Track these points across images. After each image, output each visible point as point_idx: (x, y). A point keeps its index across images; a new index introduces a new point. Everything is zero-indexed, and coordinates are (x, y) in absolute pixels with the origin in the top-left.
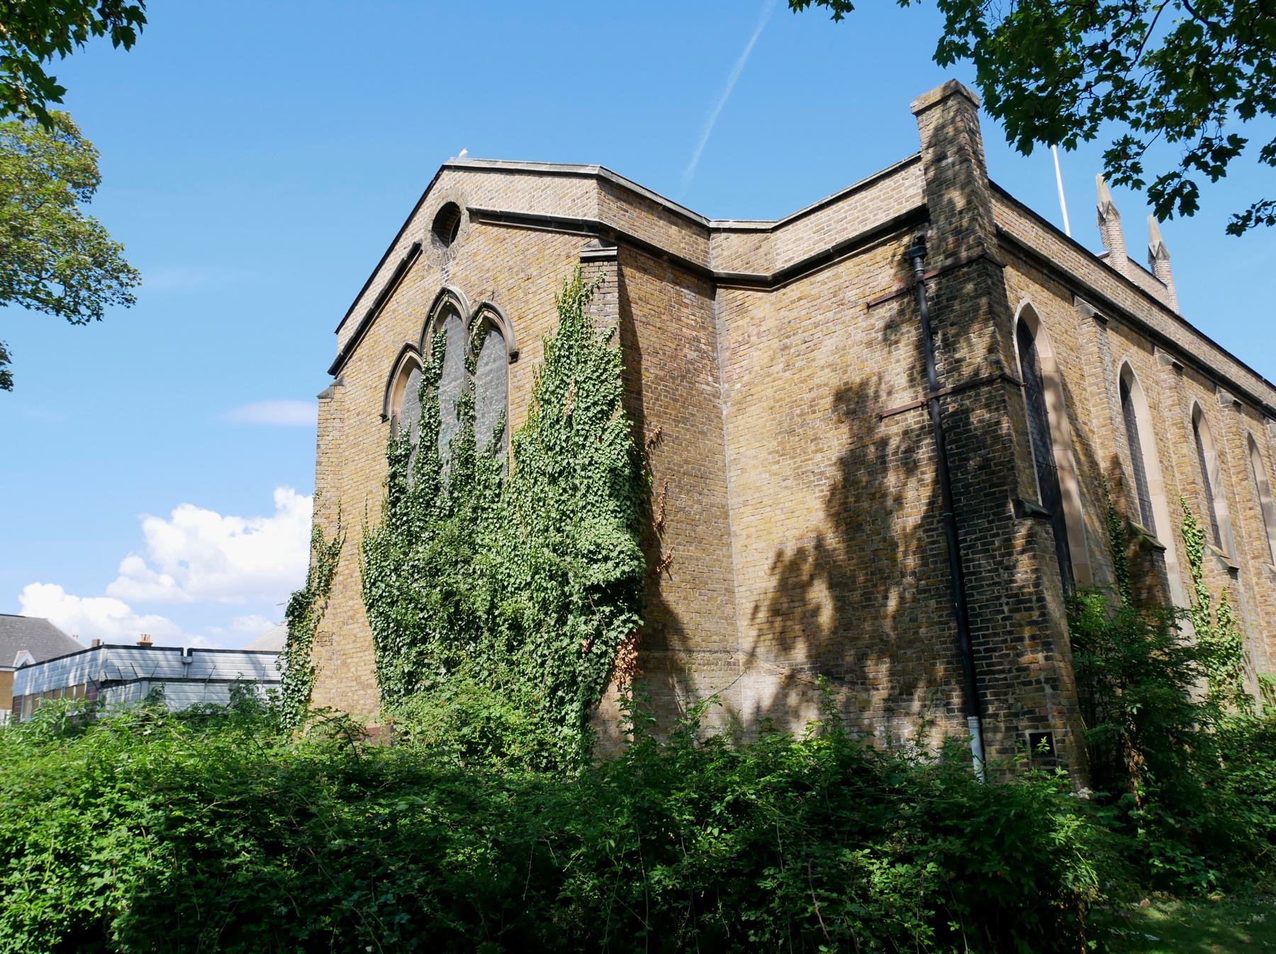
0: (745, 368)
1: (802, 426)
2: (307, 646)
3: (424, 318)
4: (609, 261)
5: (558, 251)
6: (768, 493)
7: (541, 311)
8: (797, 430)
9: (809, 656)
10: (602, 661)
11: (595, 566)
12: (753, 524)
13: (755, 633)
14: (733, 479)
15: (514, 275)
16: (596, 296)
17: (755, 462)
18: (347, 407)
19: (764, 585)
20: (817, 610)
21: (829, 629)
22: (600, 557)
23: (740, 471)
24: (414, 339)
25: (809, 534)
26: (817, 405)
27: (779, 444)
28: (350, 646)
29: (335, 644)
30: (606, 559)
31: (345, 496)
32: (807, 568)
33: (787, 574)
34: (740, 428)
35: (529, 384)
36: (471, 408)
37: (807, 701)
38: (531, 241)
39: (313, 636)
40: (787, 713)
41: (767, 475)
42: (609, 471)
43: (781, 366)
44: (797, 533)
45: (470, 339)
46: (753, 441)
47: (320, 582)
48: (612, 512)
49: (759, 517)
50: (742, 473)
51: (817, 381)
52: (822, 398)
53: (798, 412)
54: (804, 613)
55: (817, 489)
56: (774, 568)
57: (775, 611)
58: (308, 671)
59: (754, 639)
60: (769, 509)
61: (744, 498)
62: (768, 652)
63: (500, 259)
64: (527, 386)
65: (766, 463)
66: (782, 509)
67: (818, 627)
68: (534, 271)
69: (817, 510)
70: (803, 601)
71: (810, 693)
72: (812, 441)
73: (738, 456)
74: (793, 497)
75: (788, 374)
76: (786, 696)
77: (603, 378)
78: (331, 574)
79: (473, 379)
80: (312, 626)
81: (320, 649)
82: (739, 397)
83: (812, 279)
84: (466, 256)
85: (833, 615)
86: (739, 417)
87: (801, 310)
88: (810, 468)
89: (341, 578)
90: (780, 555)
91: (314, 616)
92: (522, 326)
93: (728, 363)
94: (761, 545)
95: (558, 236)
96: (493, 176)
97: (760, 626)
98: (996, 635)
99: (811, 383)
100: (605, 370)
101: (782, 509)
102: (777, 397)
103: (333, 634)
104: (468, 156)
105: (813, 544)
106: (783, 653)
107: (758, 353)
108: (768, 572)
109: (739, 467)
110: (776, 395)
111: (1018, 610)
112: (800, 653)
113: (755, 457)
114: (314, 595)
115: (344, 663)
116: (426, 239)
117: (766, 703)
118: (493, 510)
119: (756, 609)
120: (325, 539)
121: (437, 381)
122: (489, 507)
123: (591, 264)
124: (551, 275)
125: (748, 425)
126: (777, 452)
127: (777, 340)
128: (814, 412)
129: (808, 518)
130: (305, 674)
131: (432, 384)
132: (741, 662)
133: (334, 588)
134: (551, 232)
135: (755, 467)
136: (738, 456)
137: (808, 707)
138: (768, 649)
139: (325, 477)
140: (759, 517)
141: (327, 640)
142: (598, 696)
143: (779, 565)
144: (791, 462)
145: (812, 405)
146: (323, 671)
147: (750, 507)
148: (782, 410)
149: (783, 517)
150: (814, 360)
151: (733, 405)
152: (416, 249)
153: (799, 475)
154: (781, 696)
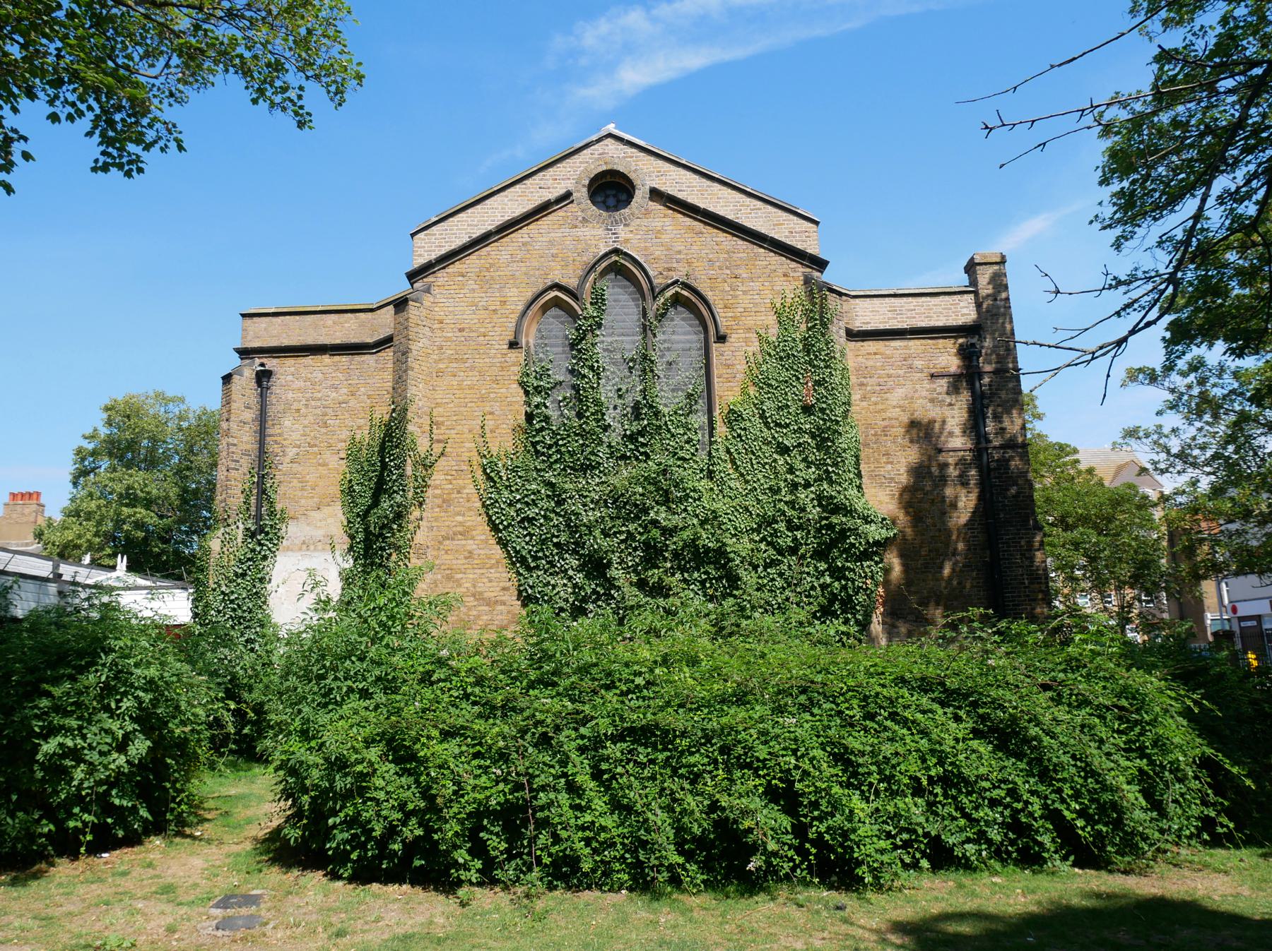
5: (773, 267)
7: (754, 309)
24: (572, 283)
31: (441, 409)
43: (859, 396)
52: (893, 427)
68: (743, 273)
75: (864, 404)
83: (887, 343)
87: (877, 362)
89: (438, 492)
92: (730, 314)
95: (772, 254)
98: (1020, 596)
99: (884, 415)
111: (1033, 583)
116: (578, 191)
124: (766, 284)
145: (885, 429)
152: (567, 196)
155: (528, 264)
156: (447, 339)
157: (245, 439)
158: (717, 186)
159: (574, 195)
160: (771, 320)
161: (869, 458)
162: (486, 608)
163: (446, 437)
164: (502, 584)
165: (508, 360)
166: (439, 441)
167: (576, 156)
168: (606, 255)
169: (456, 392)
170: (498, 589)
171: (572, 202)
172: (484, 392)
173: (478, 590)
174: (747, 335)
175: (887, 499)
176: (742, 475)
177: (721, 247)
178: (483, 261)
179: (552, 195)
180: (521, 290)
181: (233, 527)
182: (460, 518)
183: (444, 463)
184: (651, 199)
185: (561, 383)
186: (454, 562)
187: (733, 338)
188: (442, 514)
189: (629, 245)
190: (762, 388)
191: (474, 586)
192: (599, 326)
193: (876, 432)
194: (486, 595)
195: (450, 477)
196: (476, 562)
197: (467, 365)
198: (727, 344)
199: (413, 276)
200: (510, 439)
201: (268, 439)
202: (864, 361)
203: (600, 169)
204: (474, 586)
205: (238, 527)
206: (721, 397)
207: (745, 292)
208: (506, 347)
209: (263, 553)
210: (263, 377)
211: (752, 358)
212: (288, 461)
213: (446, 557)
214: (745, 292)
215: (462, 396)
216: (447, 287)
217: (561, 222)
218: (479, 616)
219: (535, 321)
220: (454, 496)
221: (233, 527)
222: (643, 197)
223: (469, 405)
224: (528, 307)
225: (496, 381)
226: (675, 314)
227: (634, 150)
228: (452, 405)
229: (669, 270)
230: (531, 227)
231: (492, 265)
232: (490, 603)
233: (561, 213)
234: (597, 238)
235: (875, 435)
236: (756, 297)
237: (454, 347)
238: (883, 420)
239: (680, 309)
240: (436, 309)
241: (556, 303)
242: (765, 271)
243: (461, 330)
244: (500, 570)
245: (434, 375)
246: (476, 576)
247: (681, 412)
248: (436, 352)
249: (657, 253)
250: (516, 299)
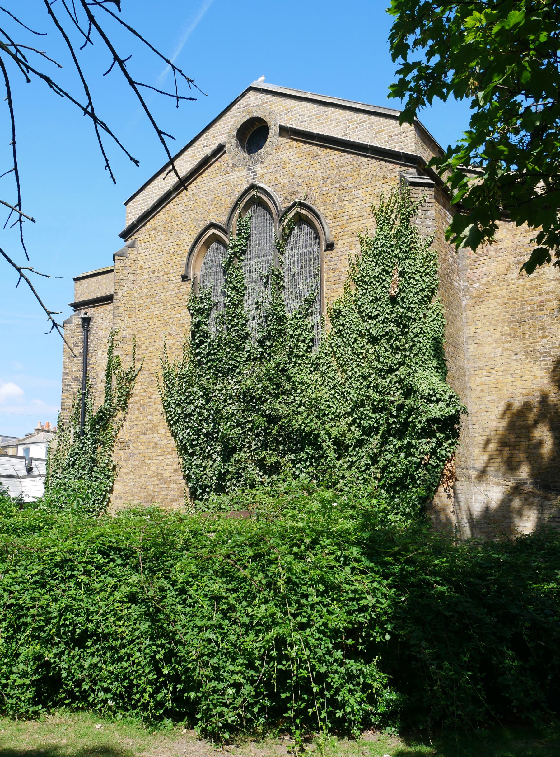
0: (483, 273)
1: (531, 319)
2: (110, 449)
3: (230, 206)
4: (429, 187)
5: (375, 173)
6: (500, 362)
7: (357, 215)
8: (527, 321)
9: (531, 475)
10: (436, 470)
11: (432, 405)
12: (486, 383)
13: (486, 457)
14: (469, 350)
15: (328, 184)
16: (420, 212)
17: (490, 340)
18: (139, 265)
19: (494, 425)
20: (540, 444)
21: (548, 457)
22: (435, 398)
23: (476, 345)
24: (222, 220)
25: (534, 393)
26: (545, 305)
27: (511, 329)
28: (149, 451)
29: (131, 448)
30: (438, 401)
31: (140, 335)
32: (532, 416)
33: (515, 419)
34: (477, 315)
35: (345, 269)
36: (282, 280)
37: (528, 504)
38: (346, 161)
39: (114, 441)
40: (511, 512)
41: (500, 350)
42: (433, 339)
44: (524, 391)
45: (281, 228)
46: (488, 325)
47: (120, 401)
48: (435, 368)
49: (492, 378)
50: (478, 346)
51: (545, 289)
53: (529, 308)
54: (528, 446)
55: (543, 363)
56: (504, 414)
57: (503, 443)
58: (110, 468)
59: (486, 461)
60: (501, 373)
61: (479, 364)
62: (498, 470)
63: (312, 169)
64: (343, 269)
65: (499, 341)
66: (512, 374)
67: (540, 456)
68: (350, 184)
69: (541, 377)
70: (529, 439)
71: (531, 499)
72: (539, 329)
73: (475, 334)
74: (522, 367)
76: (511, 500)
77: (427, 272)
78: (128, 394)
79: (281, 257)
80: (114, 433)
81: (120, 451)
82: (477, 293)
84: (275, 162)
85: (552, 448)
86: (477, 307)
88: (537, 348)
89: (137, 398)
90: (509, 406)
91: (115, 427)
92: (337, 224)
93: (469, 267)
94: (493, 397)
95: (374, 161)
96: (304, 104)
97: (490, 453)
99: (540, 290)
100: (428, 267)
101: (512, 374)
102: (511, 296)
103: (130, 441)
104: (265, 81)
105: (538, 399)
106: (510, 472)
107: (495, 263)
108: (499, 416)
109: (475, 342)
110: (510, 295)
112: (524, 472)
113: (490, 336)
114: (115, 409)
115: (143, 463)
116: (229, 142)
117: (494, 504)
118: (307, 357)
119: (488, 441)
120: (123, 367)
121: (241, 255)
122: (304, 355)
123: (417, 188)
124: (368, 189)
125: (485, 314)
126: (509, 335)
127: (512, 256)
128: (542, 310)
129: (534, 381)
130: (109, 470)
131: (237, 257)
132: (473, 476)
133: (130, 406)
134: (367, 157)
135: (489, 343)
136: (475, 334)
137: (530, 509)
138: (496, 468)
139: (122, 319)
140: (492, 378)
141: (125, 445)
142: (433, 494)
143: (508, 412)
144: (521, 342)
145: (541, 305)
146: (122, 469)
147: (484, 371)
148: (515, 306)
149: (513, 380)
150: (544, 274)
151: (471, 298)
152: (220, 149)
153: (528, 352)
154: (507, 500)
155: (195, 211)
156: (145, 281)
157: (74, 368)
158: (331, 109)
159: (227, 146)
160: (371, 222)
161: (524, 334)
162: (164, 486)
163: (143, 356)
164: (174, 467)
165: (181, 290)
166: (139, 360)
167: (228, 113)
168: (246, 192)
169: (149, 320)
170: (172, 471)
171: (225, 152)
172: (166, 318)
173: (160, 472)
174: (351, 240)
175: (541, 373)
176: (342, 366)
177: (333, 164)
178: (167, 215)
179: (208, 151)
180: (190, 233)
181: (67, 431)
182: (149, 418)
183: (141, 377)
184: (281, 135)
185: (217, 303)
186: (146, 451)
187: (339, 246)
188: (140, 415)
189: (263, 179)
190: (360, 286)
191: (158, 469)
192: (244, 252)
193: (532, 308)
194: (165, 475)
195: (144, 387)
196: (159, 450)
197: (156, 299)
198: (334, 250)
199: (125, 235)
200: (181, 353)
201: (88, 366)
202: (521, 239)
203: (245, 119)
204: (158, 469)
205: (70, 432)
206: (328, 299)
207: (350, 201)
208: (180, 280)
209: (84, 449)
210: (86, 321)
211: (354, 260)
212: (100, 381)
213: (141, 447)
214: (350, 201)
215: (153, 323)
216: (145, 241)
217: (217, 172)
218: (160, 492)
219: (201, 256)
220: (146, 401)
221: (67, 431)
222: (275, 135)
223: (157, 329)
224: (194, 246)
225: (174, 309)
226: (299, 231)
227: (269, 96)
228: (146, 331)
229: (292, 194)
230: (198, 180)
231: (172, 217)
232: (167, 482)
233: (217, 164)
234: (241, 178)
235: (531, 311)
236: (359, 203)
237: (148, 286)
238: (540, 294)
239: (302, 226)
240: (139, 259)
241: (215, 239)
242: (367, 178)
243: (153, 272)
244: (174, 456)
245: (137, 309)
246: (158, 461)
247: (299, 316)
248: (138, 292)
249: (283, 181)
250: (187, 241)
